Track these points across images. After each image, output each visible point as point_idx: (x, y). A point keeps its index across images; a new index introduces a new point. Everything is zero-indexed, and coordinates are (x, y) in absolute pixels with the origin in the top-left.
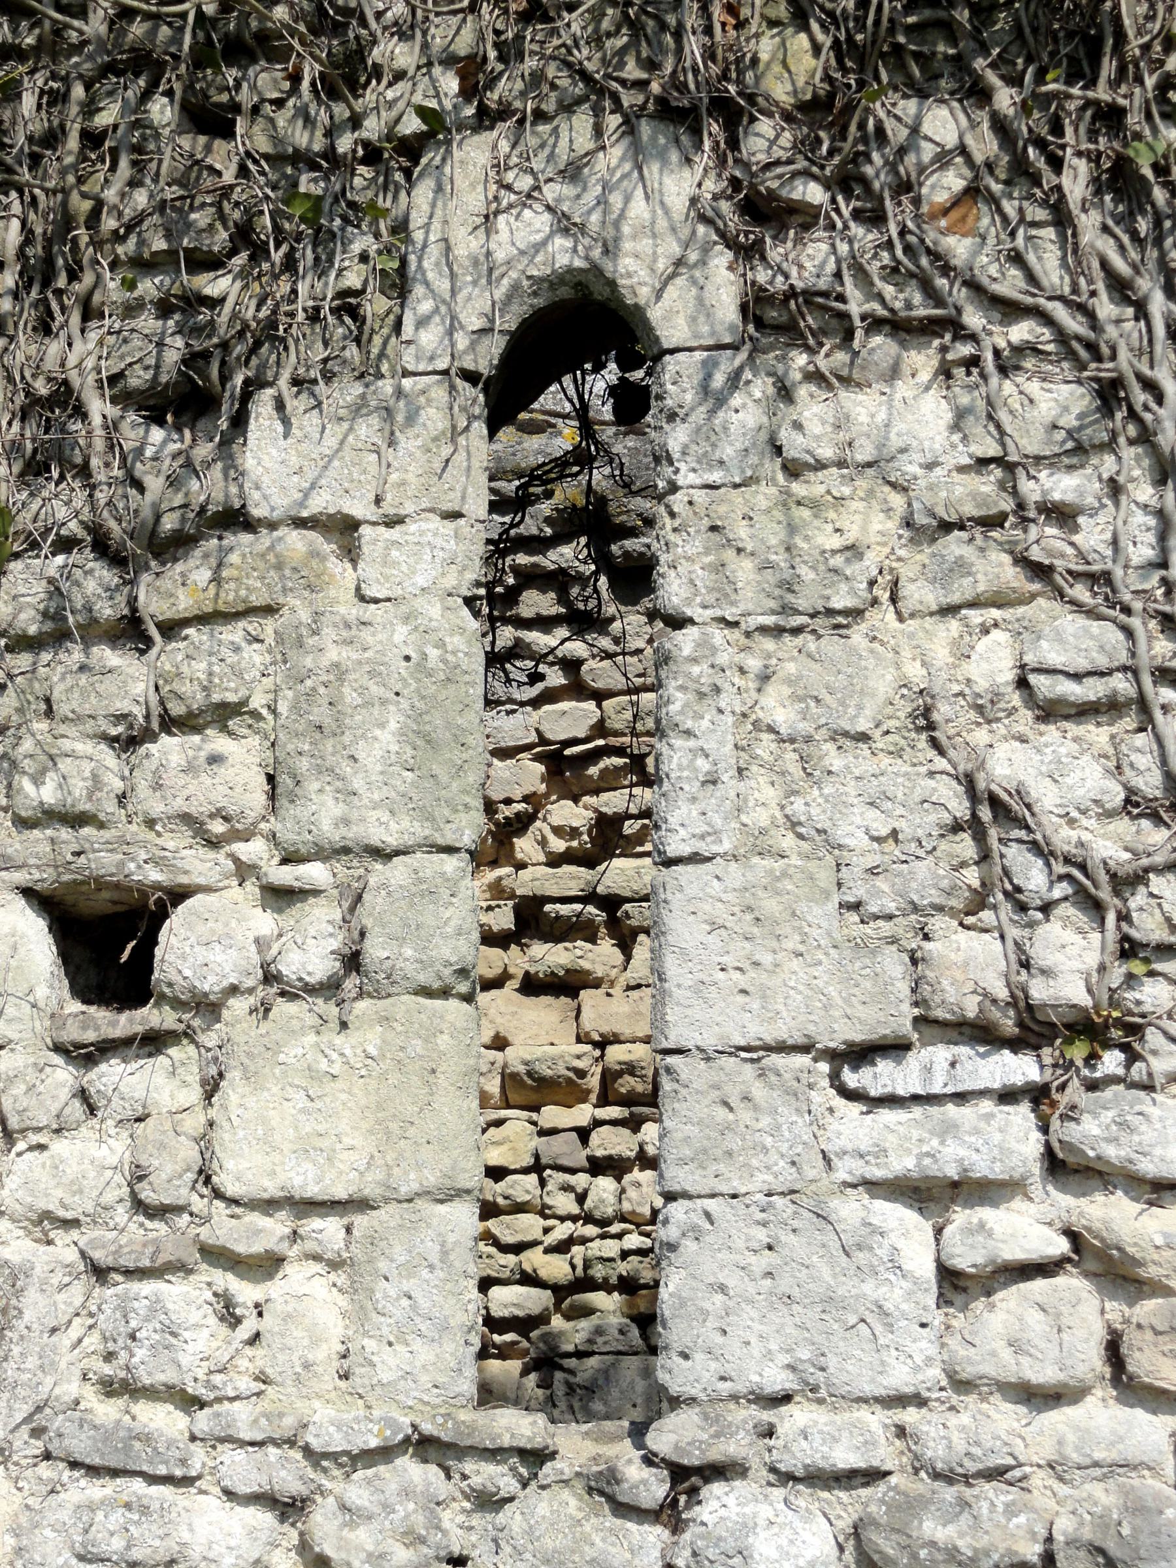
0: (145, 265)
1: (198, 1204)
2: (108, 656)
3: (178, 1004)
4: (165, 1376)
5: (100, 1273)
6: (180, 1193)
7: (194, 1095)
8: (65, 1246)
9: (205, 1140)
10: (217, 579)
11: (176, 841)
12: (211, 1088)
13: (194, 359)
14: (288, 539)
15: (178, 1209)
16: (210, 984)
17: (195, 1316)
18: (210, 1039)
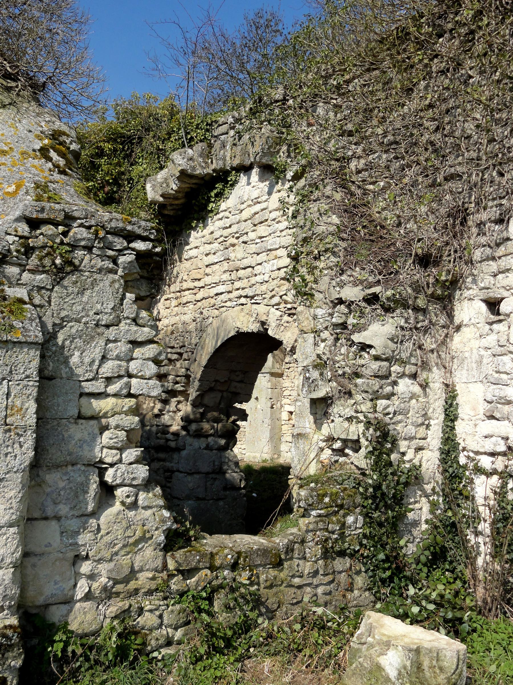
0: (494, 199)
1: (508, 345)
2: (491, 262)
3: (504, 315)
4: (504, 370)
5: (494, 355)
6: (505, 343)
7: (507, 328)
8: (489, 352)
9: (508, 335)
10: (506, 249)
11: (502, 291)
12: (509, 327)
13: (501, 214)
14: (67, 509)
15: (505, 346)
16: (507, 312)
17: (508, 361)
18: (509, 320)
